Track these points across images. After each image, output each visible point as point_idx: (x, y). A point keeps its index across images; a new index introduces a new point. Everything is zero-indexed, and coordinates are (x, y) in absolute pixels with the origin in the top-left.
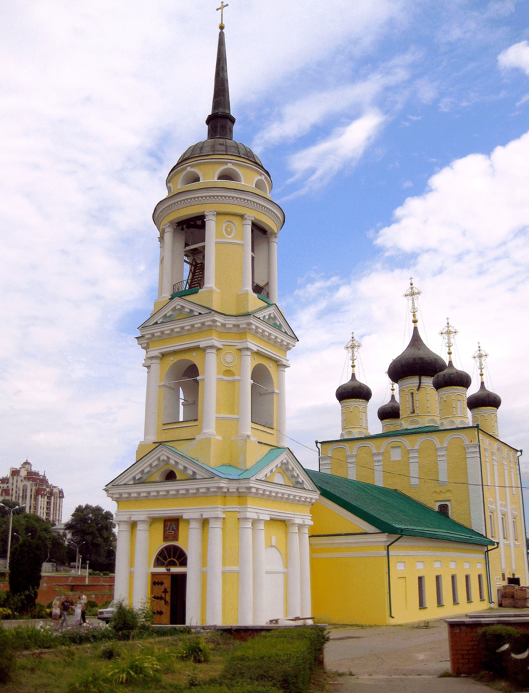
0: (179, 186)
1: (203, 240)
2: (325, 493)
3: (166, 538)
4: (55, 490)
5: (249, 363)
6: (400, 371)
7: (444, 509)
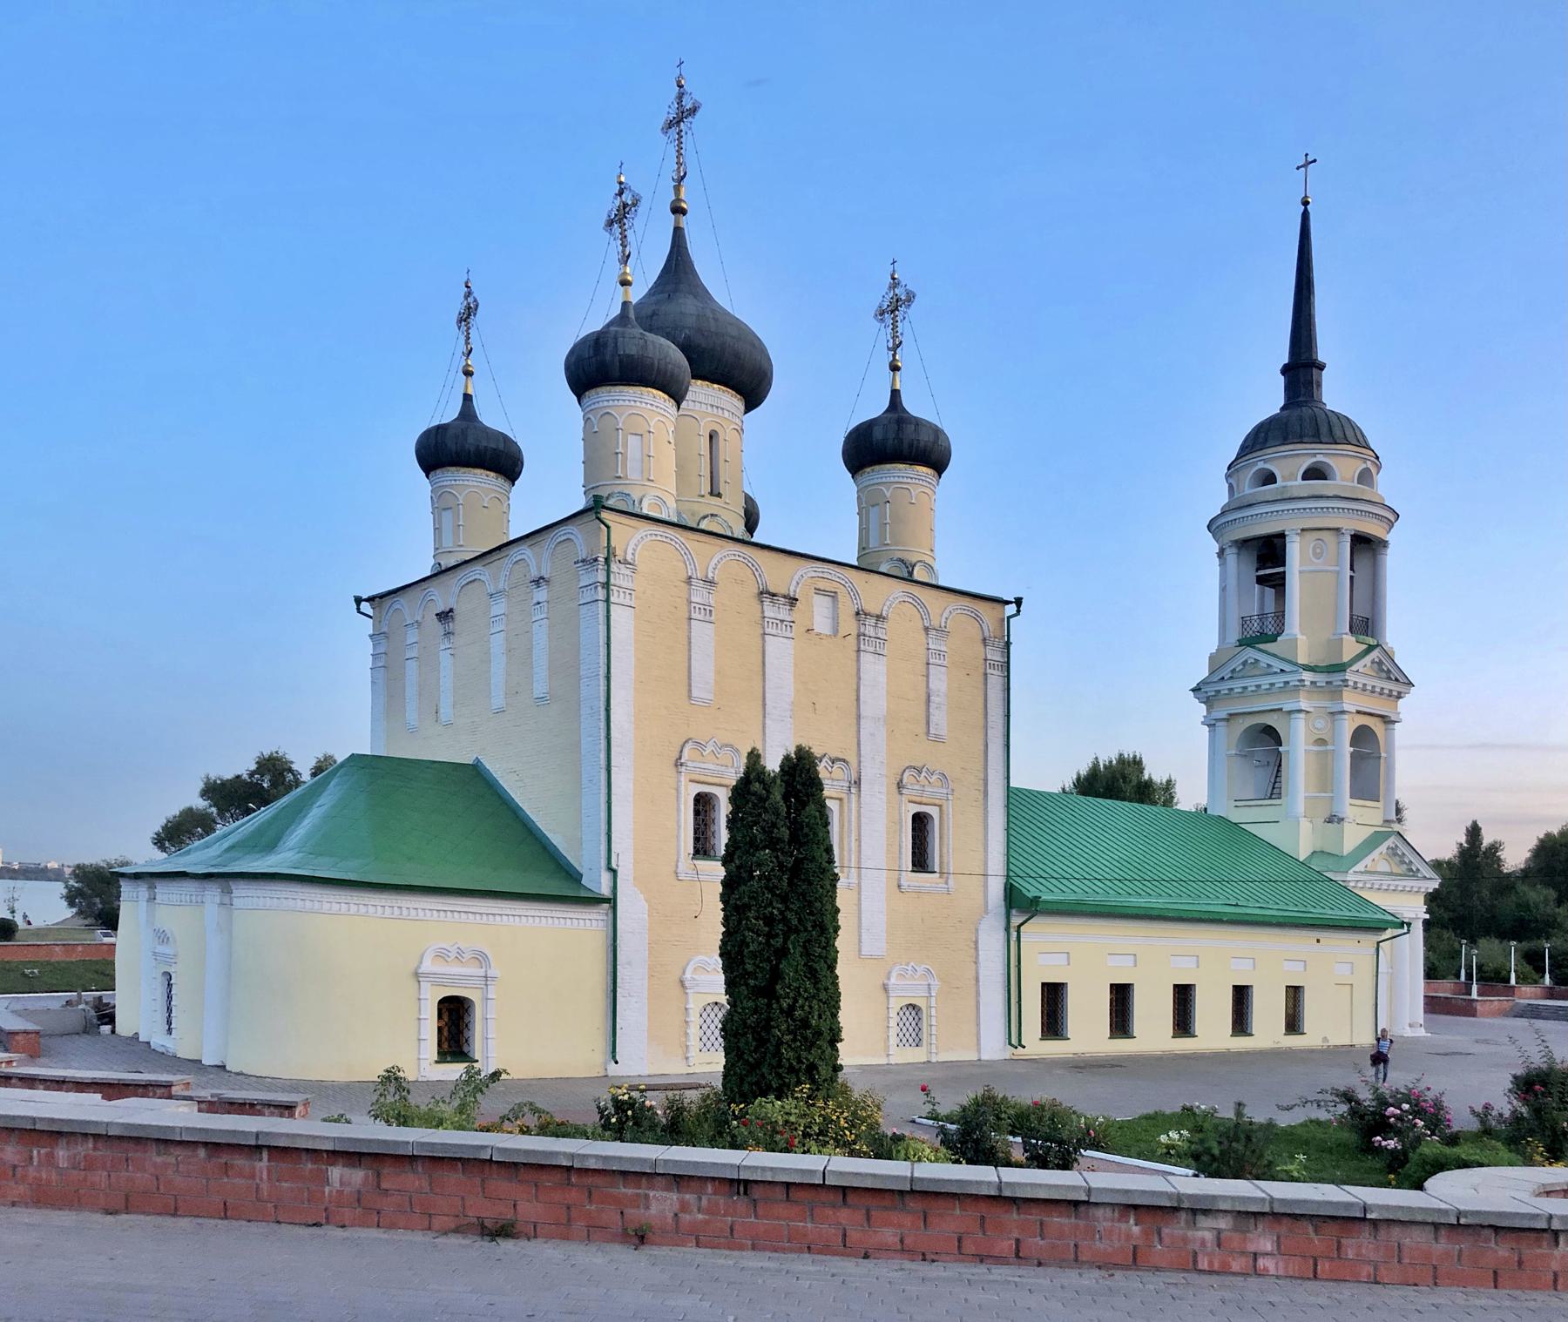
0: (1248, 489)
1: (1284, 564)
5: (1348, 726)
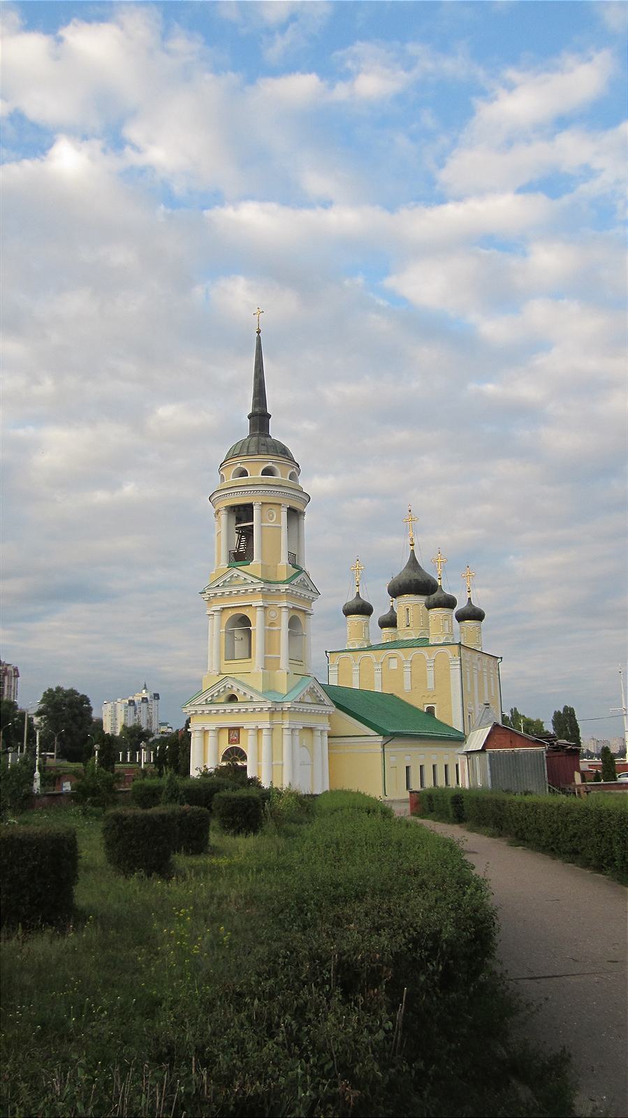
0: (231, 480)
2: (339, 706)
3: (230, 741)
4: (9, 669)
6: (397, 590)
7: (430, 711)
